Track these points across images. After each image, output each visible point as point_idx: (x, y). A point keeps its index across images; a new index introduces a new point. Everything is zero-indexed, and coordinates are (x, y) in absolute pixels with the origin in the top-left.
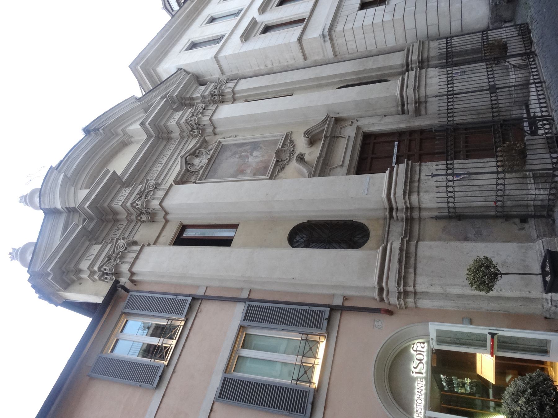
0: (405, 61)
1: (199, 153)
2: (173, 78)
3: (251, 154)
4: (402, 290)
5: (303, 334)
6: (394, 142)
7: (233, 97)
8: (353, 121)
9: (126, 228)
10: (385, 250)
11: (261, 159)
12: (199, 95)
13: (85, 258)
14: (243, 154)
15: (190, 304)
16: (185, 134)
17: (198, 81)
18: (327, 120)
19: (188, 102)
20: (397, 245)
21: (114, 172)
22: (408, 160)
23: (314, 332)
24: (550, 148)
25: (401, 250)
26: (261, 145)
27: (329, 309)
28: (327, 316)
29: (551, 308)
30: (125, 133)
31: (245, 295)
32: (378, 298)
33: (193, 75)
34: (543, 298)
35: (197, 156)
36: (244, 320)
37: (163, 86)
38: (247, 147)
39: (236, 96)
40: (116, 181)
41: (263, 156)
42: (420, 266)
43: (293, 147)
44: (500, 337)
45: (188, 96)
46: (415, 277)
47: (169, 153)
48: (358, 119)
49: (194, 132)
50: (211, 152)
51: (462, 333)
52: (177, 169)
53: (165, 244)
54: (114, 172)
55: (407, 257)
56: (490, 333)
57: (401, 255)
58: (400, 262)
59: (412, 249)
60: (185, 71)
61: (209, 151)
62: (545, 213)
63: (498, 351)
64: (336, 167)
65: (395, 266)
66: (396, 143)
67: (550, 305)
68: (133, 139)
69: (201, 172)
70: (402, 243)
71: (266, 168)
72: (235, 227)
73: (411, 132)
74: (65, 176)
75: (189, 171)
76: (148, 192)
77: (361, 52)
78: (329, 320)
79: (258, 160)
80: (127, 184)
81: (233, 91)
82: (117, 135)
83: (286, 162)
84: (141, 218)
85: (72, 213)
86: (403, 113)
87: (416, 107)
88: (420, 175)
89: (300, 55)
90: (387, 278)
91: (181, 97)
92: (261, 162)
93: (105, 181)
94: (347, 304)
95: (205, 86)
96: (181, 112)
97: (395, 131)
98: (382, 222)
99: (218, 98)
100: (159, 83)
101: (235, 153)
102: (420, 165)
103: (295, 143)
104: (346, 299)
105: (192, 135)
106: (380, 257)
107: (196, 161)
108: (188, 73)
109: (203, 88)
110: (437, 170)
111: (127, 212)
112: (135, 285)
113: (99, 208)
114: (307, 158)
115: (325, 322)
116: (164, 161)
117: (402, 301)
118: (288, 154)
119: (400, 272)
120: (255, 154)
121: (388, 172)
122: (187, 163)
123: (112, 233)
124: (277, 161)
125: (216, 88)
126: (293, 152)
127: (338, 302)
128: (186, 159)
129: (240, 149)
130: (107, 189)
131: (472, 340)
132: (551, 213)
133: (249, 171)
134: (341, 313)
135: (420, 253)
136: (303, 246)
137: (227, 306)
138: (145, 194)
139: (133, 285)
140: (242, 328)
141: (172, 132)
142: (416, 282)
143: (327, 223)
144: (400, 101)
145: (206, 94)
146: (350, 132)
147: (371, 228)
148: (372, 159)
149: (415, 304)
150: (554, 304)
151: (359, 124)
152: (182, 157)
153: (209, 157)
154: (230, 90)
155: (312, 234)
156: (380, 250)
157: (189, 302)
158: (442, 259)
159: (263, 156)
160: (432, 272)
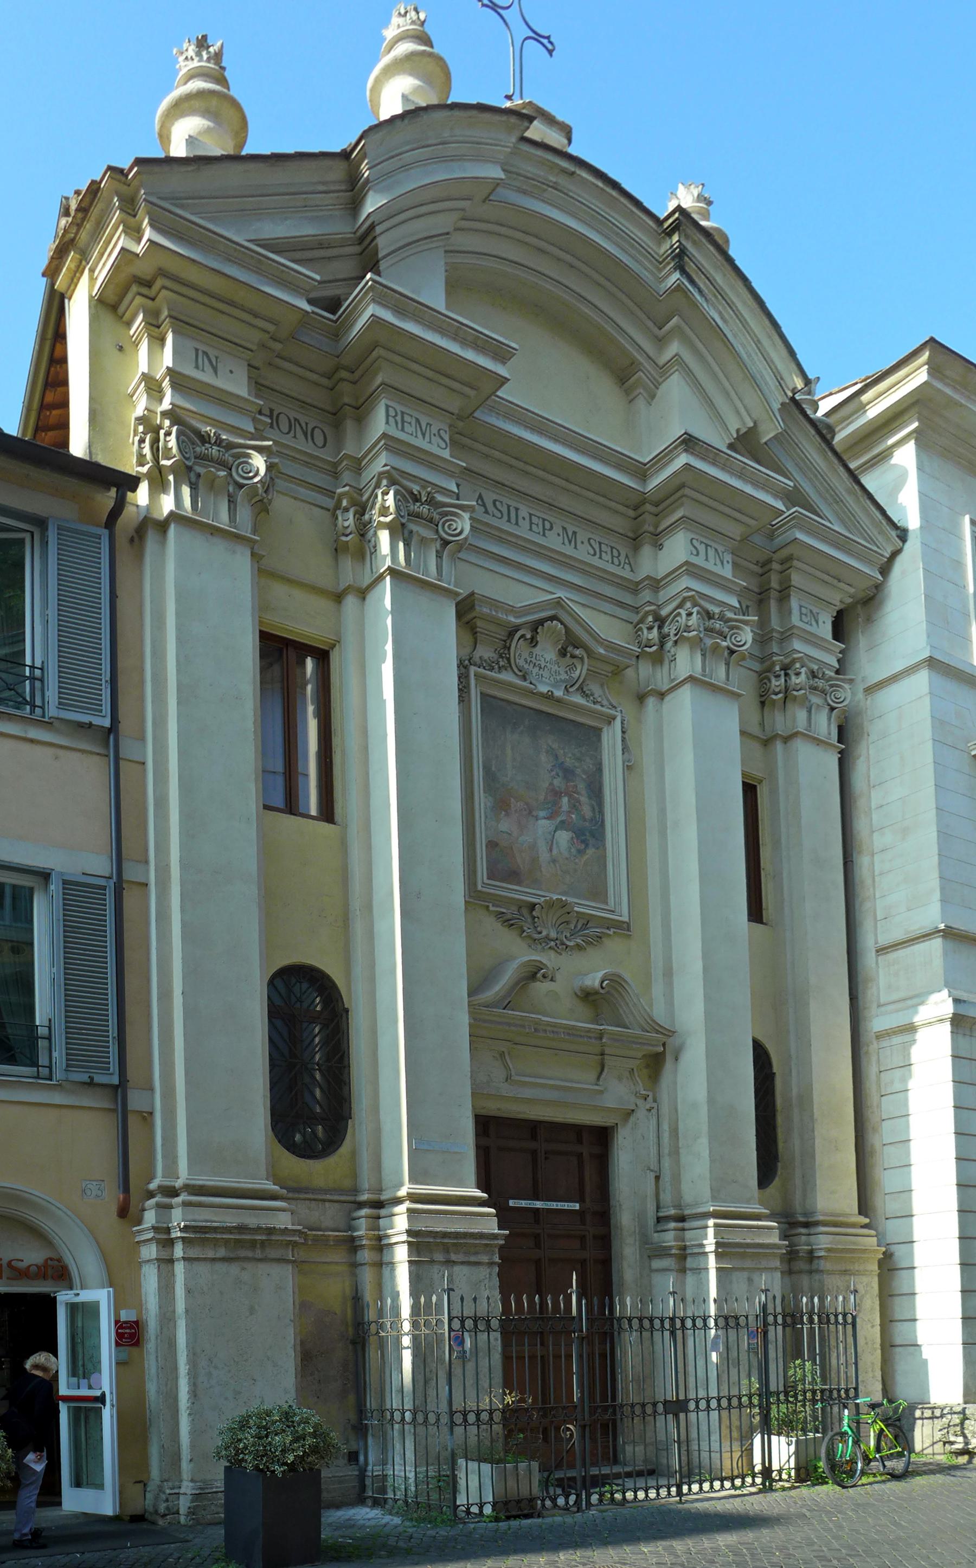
0: (821, 1218)
1: (573, 656)
2: (869, 515)
3: (563, 825)
4: (173, 1235)
5: (50, 1028)
6: (581, 1200)
7: (776, 736)
8: (650, 1099)
9: (310, 462)
10: (274, 1197)
11: (544, 856)
12: (795, 620)
13: (202, 347)
14: (565, 800)
15: (90, 725)
16: (646, 595)
17: (852, 606)
18: (657, 1032)
19: (774, 584)
20: (283, 1221)
21: (504, 381)
22: (507, 1237)
23: (49, 612)
24: (506, 1503)
25: (271, 1231)
26: (590, 851)
27: (115, 1080)
28: (99, 1079)
29: (164, 1493)
30: (664, 370)
31: (131, 873)
32: (153, 1186)
33: (878, 588)
34: (181, 1481)
35: (563, 653)
36: (65, 882)
37: (840, 481)
38: (587, 811)
39: (779, 746)
40: (472, 393)
41: (554, 861)
42: (234, 1269)
43: (578, 945)
44: (99, 1412)
45: (796, 579)
46: (205, 1259)
47: (582, 553)
48: (654, 1111)
49: (650, 629)
50: (578, 699)
51: (98, 1347)
52: (516, 594)
53: (262, 606)
54: (504, 381)
55: (253, 1244)
56: (103, 1395)
57: (258, 1229)
58: (242, 1229)
59: (273, 1254)
60: (896, 553)
61: (581, 689)
62: (370, 1494)
63: (69, 1407)
64: (506, 1067)
65: (231, 1219)
66: (577, 1206)
67: (168, 1491)
68: (641, 403)
69: (506, 676)
70: (285, 1231)
71: (513, 876)
72: (327, 813)
73: (605, 1241)
74: (497, 183)
75: (511, 634)
76: (431, 521)
77: (879, 1106)
78: (91, 1084)
79: (542, 847)
80: (465, 432)
81: (796, 734)
82: (661, 342)
83: (529, 931)
84: (346, 510)
85: (357, 249)
86: (659, 1220)
87: (670, 1248)
88: (463, 1263)
89: (898, 934)
90: (200, 1205)
91: (790, 558)
92: (535, 860)
93: (470, 355)
94: (133, 1121)
95: (829, 636)
96: (727, 571)
97: (612, 1203)
98: (347, 1183)
99: (771, 687)
100: (852, 466)
101: (568, 773)
102: (491, 1264)
103: (590, 950)
104: (144, 1118)
105: (642, 621)
106: (250, 1186)
107: (547, 652)
108: (885, 569)
109: (826, 630)
110: (462, 1299)
111: (364, 457)
112: (132, 540)
113: (375, 354)
114: (541, 987)
115: (85, 1078)
116: (554, 541)
117: (150, 1235)
118: (553, 935)
119: (215, 1229)
120: (564, 837)
121: (478, 1193)
122: (536, 626)
123: (292, 415)
124: (532, 906)
125: (813, 675)
126: (560, 946)
127: (136, 1101)
128: (552, 618)
129: (581, 786)
130: (441, 368)
131: (83, 1365)
132: (369, 1502)
133: (504, 825)
134: (110, 1110)
135: (263, 1268)
136: (278, 1002)
137: (101, 831)
138: (424, 509)
139: (131, 532)
140: (45, 876)
141: (661, 547)
142: (196, 1263)
143: (342, 1057)
144: (694, 1211)
145: (797, 645)
146: (618, 1092)
147: (332, 1160)
148: (534, 1153)
149: (148, 1261)
150: (171, 1498)
151: (641, 1114)
152: (559, 603)
153: (559, 693)
154: (801, 725)
155: (308, 1030)
156: (271, 1186)
157: (97, 721)
158: (252, 1311)
159: (554, 861)
160: (221, 1293)
